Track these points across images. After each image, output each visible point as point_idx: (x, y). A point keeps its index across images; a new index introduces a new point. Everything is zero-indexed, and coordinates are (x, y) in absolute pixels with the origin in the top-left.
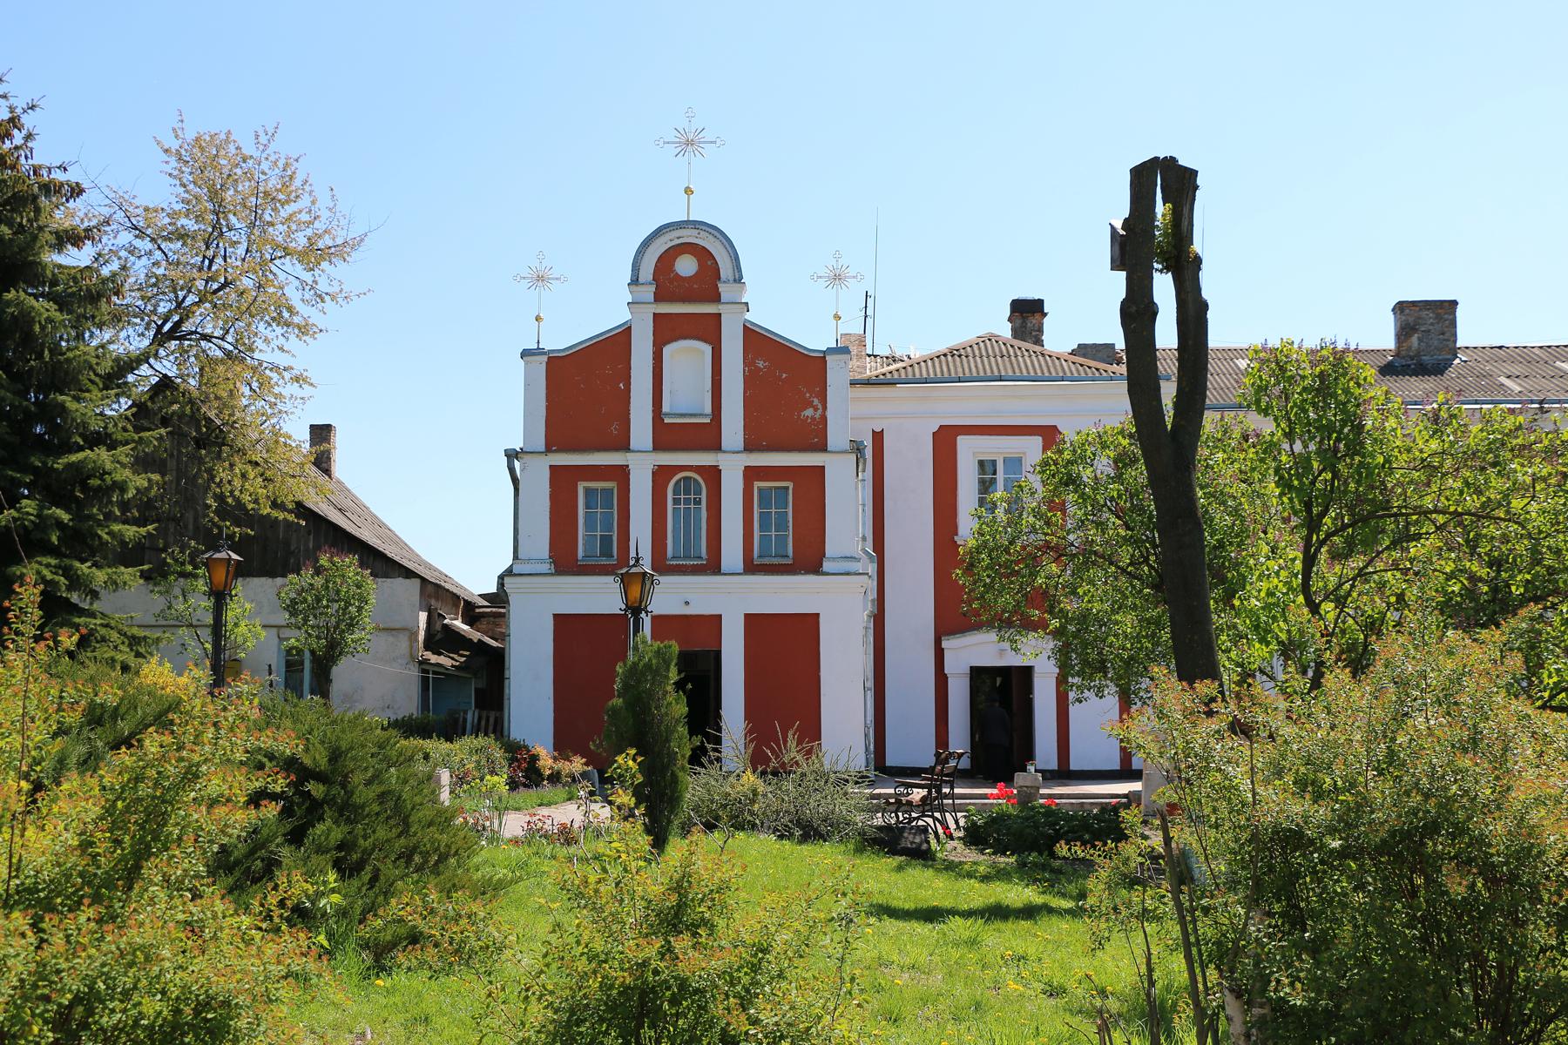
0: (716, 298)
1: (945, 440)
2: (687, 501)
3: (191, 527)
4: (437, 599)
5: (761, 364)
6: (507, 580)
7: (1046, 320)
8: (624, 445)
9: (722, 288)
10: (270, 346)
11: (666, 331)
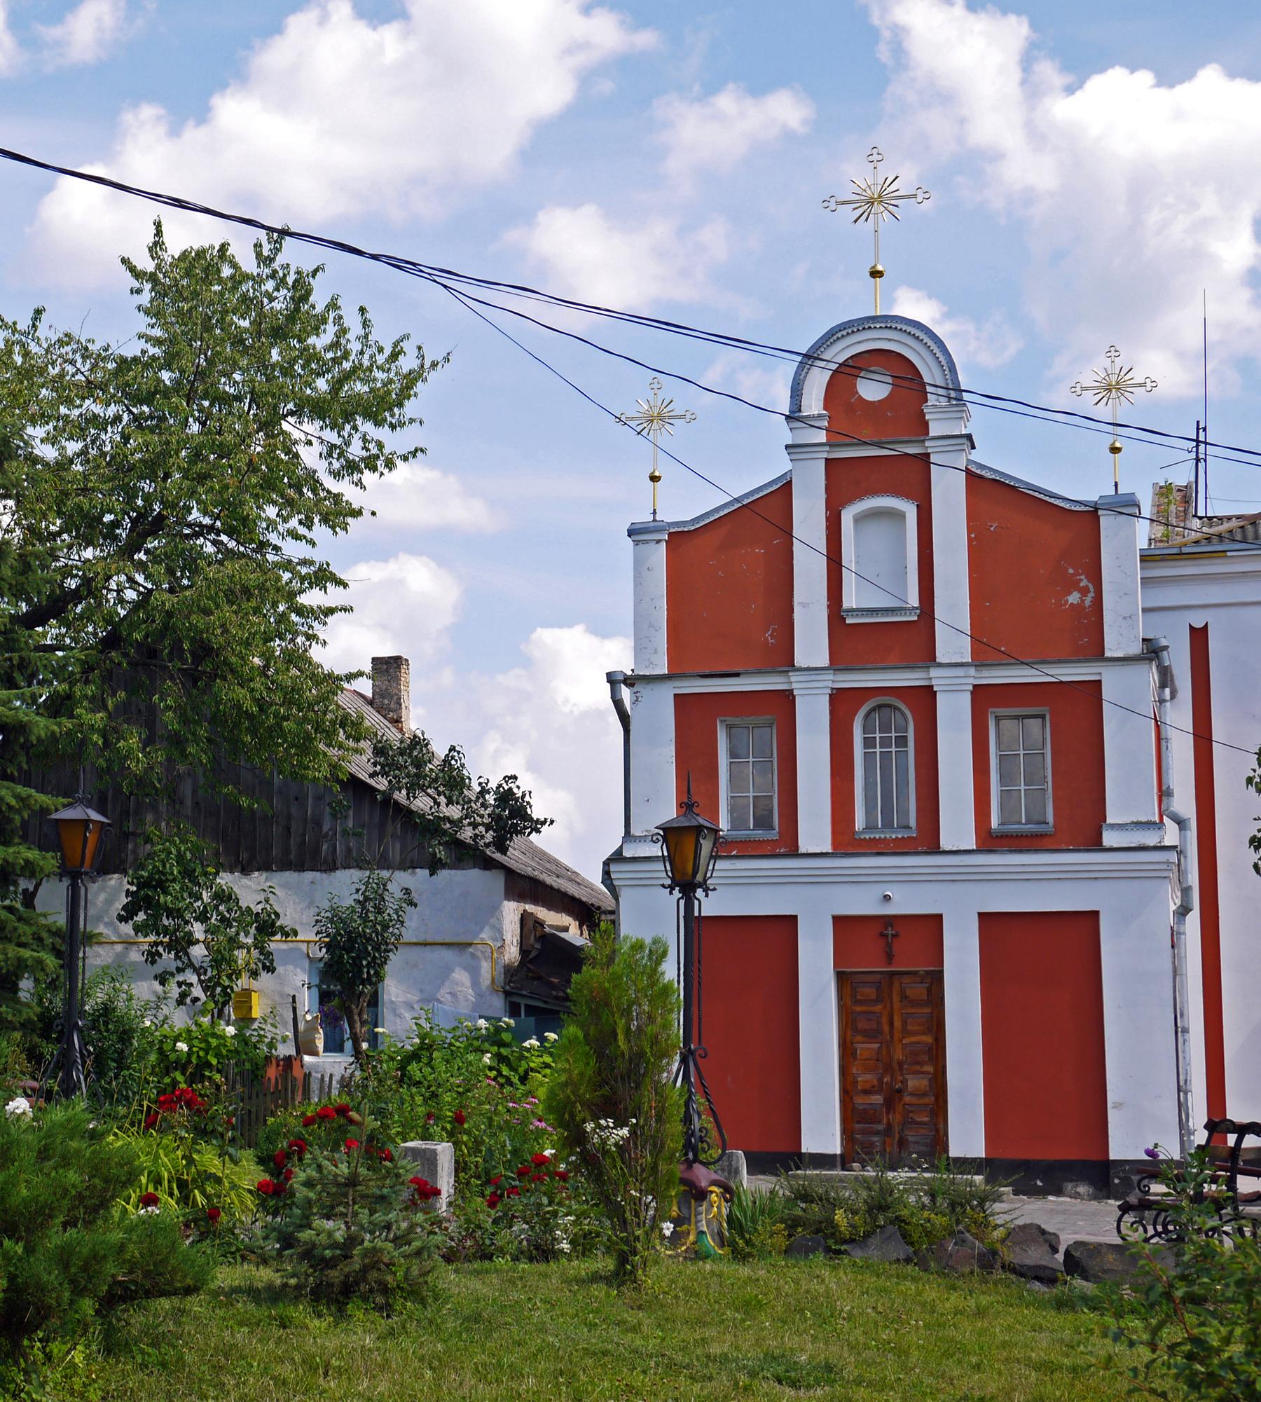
2: (885, 742)
6: (613, 868)
11: (843, 483)
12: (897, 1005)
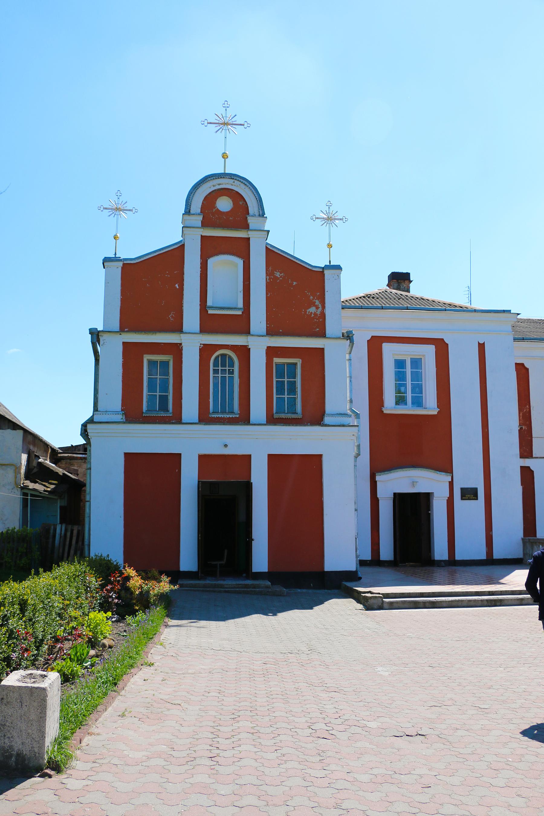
0: (246, 226)
1: (375, 345)
2: (224, 371)
4: (34, 445)
5: (278, 274)
6: (89, 426)
7: (411, 285)
8: (178, 328)
9: (250, 220)
11: (210, 248)
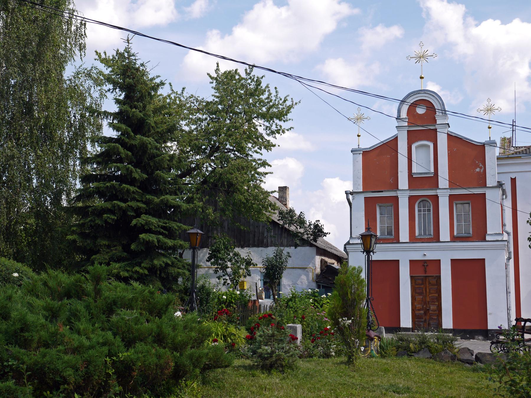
2: (424, 211)
3: (226, 228)
6: (347, 246)
10: (256, 155)
12: (427, 285)
